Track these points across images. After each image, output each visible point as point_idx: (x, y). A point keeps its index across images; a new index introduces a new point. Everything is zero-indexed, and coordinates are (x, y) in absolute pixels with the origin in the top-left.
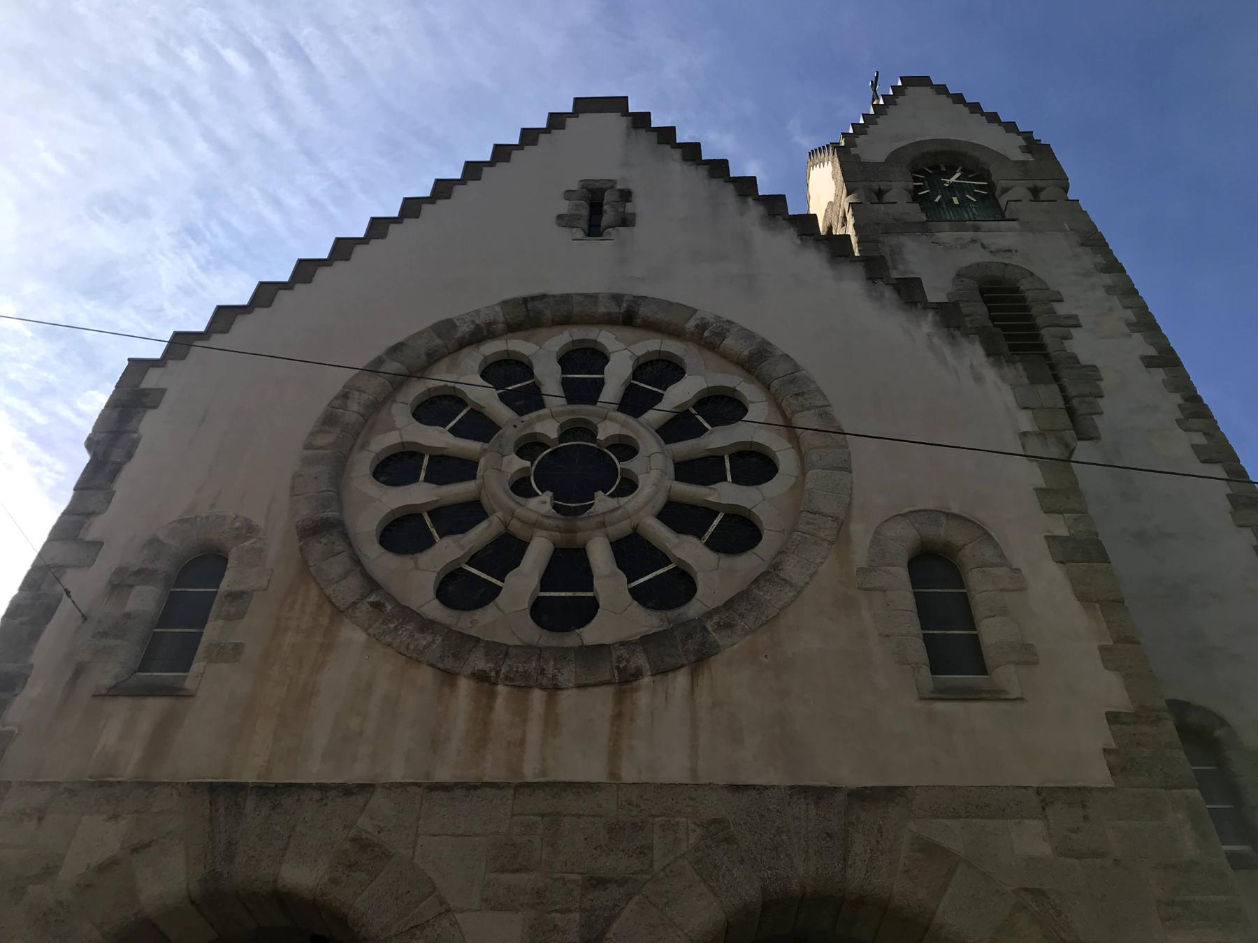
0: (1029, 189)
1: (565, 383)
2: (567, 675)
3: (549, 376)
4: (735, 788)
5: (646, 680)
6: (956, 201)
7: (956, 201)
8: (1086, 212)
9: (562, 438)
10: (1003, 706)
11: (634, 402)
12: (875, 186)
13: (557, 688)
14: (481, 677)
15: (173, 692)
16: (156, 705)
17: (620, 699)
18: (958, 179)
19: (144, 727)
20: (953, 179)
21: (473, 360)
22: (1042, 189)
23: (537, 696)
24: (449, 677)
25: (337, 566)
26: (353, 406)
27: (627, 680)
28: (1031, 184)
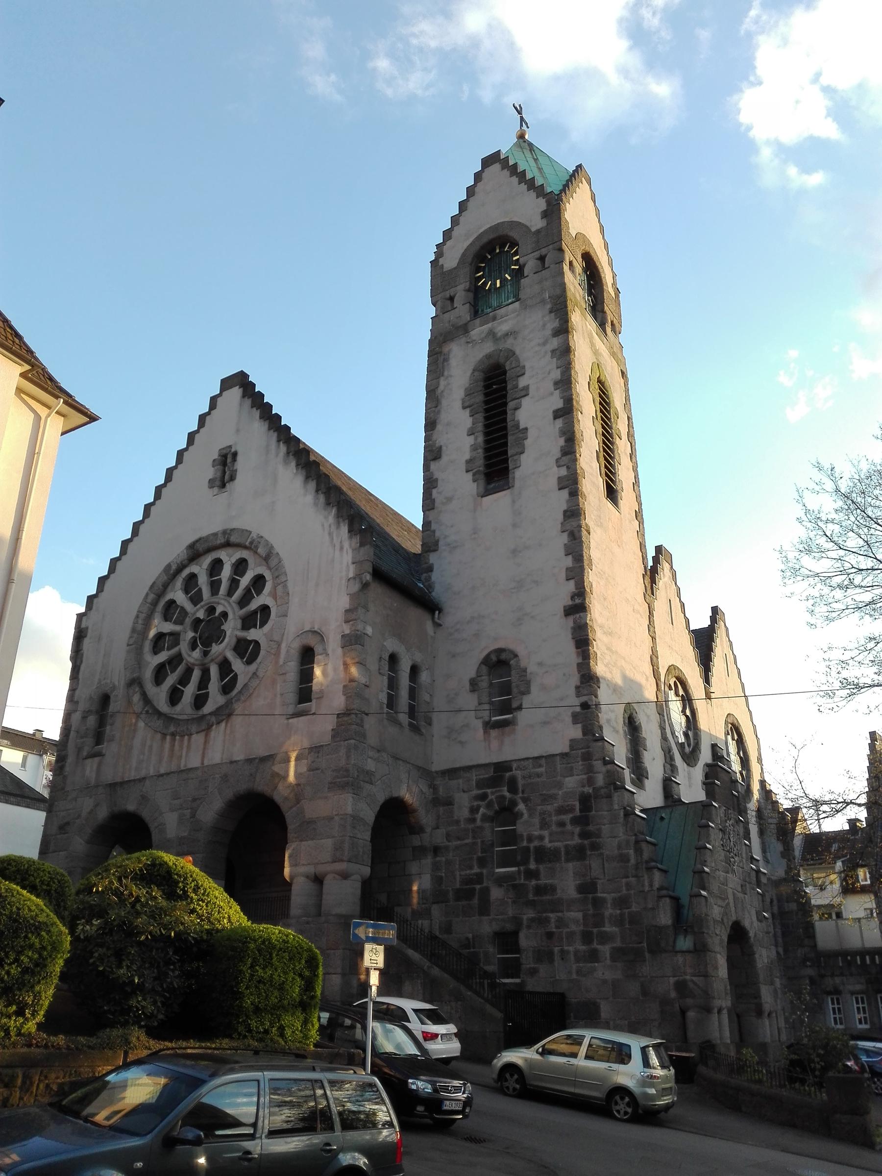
1: (176, 623)
2: (194, 728)
3: (168, 627)
4: (232, 762)
5: (214, 726)
6: (849, 958)
7: (849, 958)
9: (196, 631)
10: (308, 717)
11: (196, 599)
12: (447, 294)
13: (191, 734)
14: (173, 735)
15: (99, 754)
16: (97, 759)
17: (207, 735)
19: (95, 767)
22: (545, 256)
23: (186, 737)
24: (164, 735)
25: (136, 698)
26: (140, 621)
27: (209, 728)
28: (537, 254)
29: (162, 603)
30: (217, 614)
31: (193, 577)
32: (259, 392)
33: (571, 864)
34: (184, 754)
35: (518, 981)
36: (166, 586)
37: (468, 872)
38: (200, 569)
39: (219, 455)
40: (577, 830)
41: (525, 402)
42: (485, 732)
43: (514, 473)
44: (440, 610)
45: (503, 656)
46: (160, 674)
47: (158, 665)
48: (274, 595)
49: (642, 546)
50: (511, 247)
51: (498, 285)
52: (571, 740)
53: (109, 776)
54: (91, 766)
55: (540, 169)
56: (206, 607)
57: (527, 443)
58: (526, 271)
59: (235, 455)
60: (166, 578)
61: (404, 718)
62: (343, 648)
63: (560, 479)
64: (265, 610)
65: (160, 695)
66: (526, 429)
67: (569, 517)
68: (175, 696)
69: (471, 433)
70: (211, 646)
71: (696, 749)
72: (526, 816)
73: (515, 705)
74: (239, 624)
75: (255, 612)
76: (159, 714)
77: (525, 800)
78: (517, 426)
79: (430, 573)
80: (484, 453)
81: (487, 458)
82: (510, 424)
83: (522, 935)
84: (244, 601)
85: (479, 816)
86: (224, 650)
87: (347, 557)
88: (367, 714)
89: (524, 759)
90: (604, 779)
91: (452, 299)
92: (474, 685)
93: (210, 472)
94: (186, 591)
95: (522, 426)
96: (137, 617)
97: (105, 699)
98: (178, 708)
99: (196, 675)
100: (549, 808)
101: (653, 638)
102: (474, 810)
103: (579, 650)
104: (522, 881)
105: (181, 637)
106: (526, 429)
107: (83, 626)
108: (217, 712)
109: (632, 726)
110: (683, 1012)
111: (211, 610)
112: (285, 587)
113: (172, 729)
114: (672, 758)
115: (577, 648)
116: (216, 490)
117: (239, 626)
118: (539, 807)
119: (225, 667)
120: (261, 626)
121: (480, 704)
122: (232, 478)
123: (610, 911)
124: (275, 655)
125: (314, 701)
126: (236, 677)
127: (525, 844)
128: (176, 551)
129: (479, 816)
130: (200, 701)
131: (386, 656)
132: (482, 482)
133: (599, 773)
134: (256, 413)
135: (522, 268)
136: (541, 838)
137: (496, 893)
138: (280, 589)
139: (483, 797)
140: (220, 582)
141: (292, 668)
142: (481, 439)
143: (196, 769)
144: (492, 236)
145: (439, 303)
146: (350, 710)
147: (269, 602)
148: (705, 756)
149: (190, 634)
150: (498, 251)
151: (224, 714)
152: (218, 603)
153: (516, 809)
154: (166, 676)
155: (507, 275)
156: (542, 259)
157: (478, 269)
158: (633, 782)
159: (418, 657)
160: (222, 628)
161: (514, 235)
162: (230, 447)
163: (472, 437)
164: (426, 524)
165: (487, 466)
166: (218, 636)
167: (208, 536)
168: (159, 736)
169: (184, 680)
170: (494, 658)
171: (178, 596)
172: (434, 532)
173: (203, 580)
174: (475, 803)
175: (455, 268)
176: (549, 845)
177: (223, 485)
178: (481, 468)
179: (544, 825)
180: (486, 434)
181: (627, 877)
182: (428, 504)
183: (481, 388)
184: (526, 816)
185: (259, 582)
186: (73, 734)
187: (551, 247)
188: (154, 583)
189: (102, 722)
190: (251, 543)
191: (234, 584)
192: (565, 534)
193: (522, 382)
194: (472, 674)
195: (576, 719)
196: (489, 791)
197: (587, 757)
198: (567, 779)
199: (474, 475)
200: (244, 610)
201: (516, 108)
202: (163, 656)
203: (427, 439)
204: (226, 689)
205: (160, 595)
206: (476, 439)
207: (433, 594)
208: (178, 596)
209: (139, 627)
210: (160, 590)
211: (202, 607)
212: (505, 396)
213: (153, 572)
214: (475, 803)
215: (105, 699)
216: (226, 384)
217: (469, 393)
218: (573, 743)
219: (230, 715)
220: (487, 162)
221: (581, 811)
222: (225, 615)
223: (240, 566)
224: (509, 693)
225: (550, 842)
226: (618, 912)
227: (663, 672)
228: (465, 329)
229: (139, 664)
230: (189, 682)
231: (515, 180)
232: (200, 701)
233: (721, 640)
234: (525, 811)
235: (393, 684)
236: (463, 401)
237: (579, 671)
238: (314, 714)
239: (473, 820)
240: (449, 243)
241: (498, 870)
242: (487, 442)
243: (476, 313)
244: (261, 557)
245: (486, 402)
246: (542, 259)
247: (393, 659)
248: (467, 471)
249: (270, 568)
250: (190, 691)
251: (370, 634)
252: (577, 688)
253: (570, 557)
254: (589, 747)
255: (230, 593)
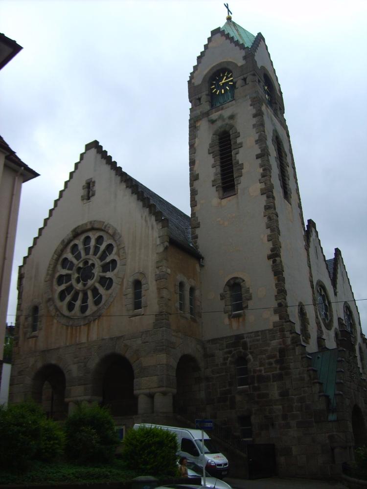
0: (242, 79)
1: (68, 269)
3: (64, 272)
5: (92, 322)
8: (201, 53)
9: (79, 274)
11: (78, 257)
12: (197, 97)
13: (81, 326)
14: (72, 326)
18: (225, 80)
20: (223, 82)
21: (56, 287)
22: (246, 78)
25: (51, 308)
28: (242, 77)
29: (61, 259)
30: (89, 265)
31: (76, 246)
32: (105, 151)
33: (275, 383)
34: (78, 335)
35: (251, 439)
36: (63, 251)
37: (224, 389)
38: (79, 242)
39: (86, 183)
40: (278, 366)
41: (241, 150)
42: (229, 318)
43: (237, 187)
44: (203, 258)
45: (237, 281)
46: (62, 296)
47: (60, 292)
48: (118, 254)
49: (303, 224)
50: (228, 74)
51: (223, 92)
52: (274, 323)
53: (41, 345)
54: (32, 342)
55: (240, 35)
56: (83, 261)
57: (244, 171)
58: (237, 85)
59: (94, 182)
60: (62, 247)
61: (188, 315)
62: (156, 281)
63: (261, 190)
64: (114, 262)
65: (63, 305)
66: (242, 164)
67: (267, 209)
68: (71, 307)
69: (214, 166)
70: (87, 281)
71: (331, 321)
72: (252, 360)
73: (244, 306)
74: (101, 269)
75: (109, 263)
76: (64, 316)
77: (251, 353)
78: (238, 162)
79: (196, 239)
80: (221, 176)
81: (222, 179)
82: (234, 162)
83: (253, 418)
84: (102, 258)
85: (228, 362)
86: (94, 283)
87: (156, 234)
88: (170, 314)
89: (250, 333)
90: (291, 341)
91: (199, 99)
92: (222, 297)
93: (82, 192)
94: (73, 252)
95: (240, 163)
96: (49, 267)
97: (36, 309)
98: (73, 312)
99: (81, 296)
100: (264, 356)
101: (310, 267)
102: (225, 359)
103: (276, 277)
104: (252, 392)
105: (72, 277)
106: (242, 164)
107: (22, 272)
108: (93, 315)
109: (302, 313)
110: (333, 449)
111: (86, 262)
112: (124, 250)
113: (71, 323)
114: (321, 327)
115: (275, 276)
116: (85, 201)
117: (101, 270)
118: (259, 356)
119: (95, 291)
120: (113, 270)
121: (226, 306)
122: (93, 195)
123: (296, 404)
124: (121, 285)
125: (143, 308)
126: (101, 296)
127: (252, 374)
128: (67, 233)
129: (228, 362)
130: (84, 309)
131: (178, 284)
132: (221, 192)
133: (288, 338)
134: (104, 161)
135: (235, 83)
136: (260, 371)
137: (238, 398)
138: (121, 251)
139: (230, 352)
140: (89, 248)
141: (130, 291)
142: (219, 169)
143: (85, 343)
144: (218, 68)
145: (193, 101)
146: (162, 312)
147: (116, 258)
148: (336, 324)
149: (76, 275)
150: (221, 75)
151: (97, 316)
152: (90, 259)
153: (247, 357)
154: (65, 297)
155: (227, 88)
156: (245, 79)
157: (212, 84)
158: (304, 341)
159: (193, 283)
160: (93, 271)
161: (230, 68)
162: (92, 178)
163: (215, 168)
164: (193, 214)
165: (223, 183)
166: (91, 276)
167: (82, 225)
168: (65, 327)
169: (75, 298)
170: (232, 282)
171: (69, 256)
172: (197, 218)
173: (81, 247)
174: (226, 356)
175: (201, 84)
176: (264, 374)
177: (89, 198)
178: (220, 184)
179: (261, 365)
180: (222, 167)
181: (304, 387)
182: (193, 203)
183: (217, 144)
184: (252, 360)
185: (110, 248)
186: (21, 327)
187: (249, 73)
188: (56, 250)
189: (35, 319)
190: (105, 227)
191: (97, 249)
192: (266, 217)
193: (239, 140)
194: (221, 291)
195: (276, 312)
196: (233, 349)
197: (282, 330)
198: (273, 342)
199: (217, 188)
200: (103, 262)
201: (225, 5)
202: (63, 287)
203: (191, 170)
204: (97, 302)
205: (60, 256)
206: (216, 170)
207: (198, 250)
208: (69, 256)
209: (50, 272)
210: (60, 252)
211: (81, 261)
212: (230, 148)
213: (56, 244)
214: (226, 356)
215: (36, 309)
216: (88, 147)
217: (211, 146)
218: (275, 324)
219: (99, 316)
220: (214, 33)
221: (280, 357)
222: (93, 265)
223: (100, 240)
224: (241, 300)
225: (265, 373)
226: (300, 404)
227: (315, 284)
228: (207, 114)
229: (52, 291)
230: (77, 300)
231: (228, 41)
232: (84, 309)
233: (340, 265)
234: (251, 358)
235: (182, 297)
236: (209, 150)
237: (276, 288)
238: (143, 315)
239: (225, 364)
240: (196, 72)
241: (239, 387)
242: (222, 171)
243: (212, 106)
244: (110, 235)
245: (220, 151)
246: (245, 79)
247: (181, 285)
248: (213, 186)
249: (115, 241)
250: (78, 303)
251: (170, 273)
252: (276, 296)
253: (269, 229)
254: (283, 325)
255: (95, 254)
